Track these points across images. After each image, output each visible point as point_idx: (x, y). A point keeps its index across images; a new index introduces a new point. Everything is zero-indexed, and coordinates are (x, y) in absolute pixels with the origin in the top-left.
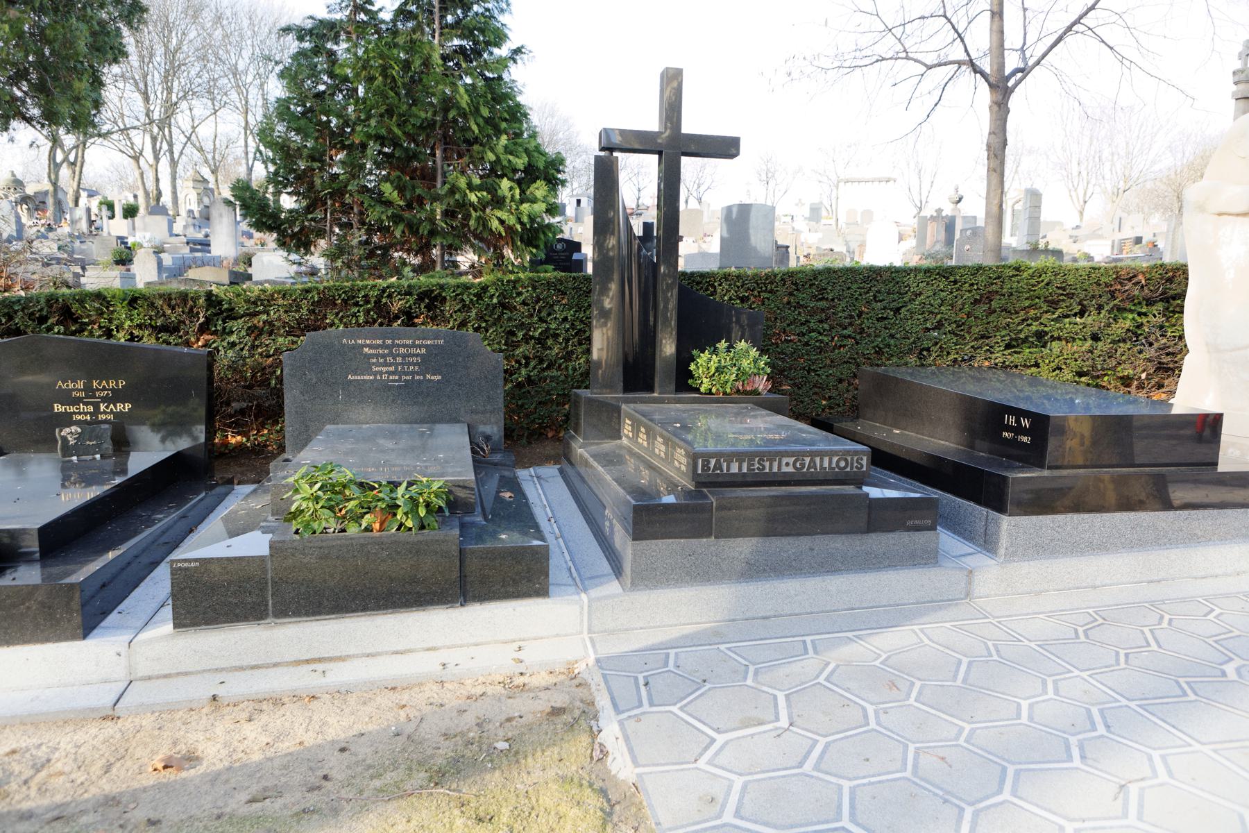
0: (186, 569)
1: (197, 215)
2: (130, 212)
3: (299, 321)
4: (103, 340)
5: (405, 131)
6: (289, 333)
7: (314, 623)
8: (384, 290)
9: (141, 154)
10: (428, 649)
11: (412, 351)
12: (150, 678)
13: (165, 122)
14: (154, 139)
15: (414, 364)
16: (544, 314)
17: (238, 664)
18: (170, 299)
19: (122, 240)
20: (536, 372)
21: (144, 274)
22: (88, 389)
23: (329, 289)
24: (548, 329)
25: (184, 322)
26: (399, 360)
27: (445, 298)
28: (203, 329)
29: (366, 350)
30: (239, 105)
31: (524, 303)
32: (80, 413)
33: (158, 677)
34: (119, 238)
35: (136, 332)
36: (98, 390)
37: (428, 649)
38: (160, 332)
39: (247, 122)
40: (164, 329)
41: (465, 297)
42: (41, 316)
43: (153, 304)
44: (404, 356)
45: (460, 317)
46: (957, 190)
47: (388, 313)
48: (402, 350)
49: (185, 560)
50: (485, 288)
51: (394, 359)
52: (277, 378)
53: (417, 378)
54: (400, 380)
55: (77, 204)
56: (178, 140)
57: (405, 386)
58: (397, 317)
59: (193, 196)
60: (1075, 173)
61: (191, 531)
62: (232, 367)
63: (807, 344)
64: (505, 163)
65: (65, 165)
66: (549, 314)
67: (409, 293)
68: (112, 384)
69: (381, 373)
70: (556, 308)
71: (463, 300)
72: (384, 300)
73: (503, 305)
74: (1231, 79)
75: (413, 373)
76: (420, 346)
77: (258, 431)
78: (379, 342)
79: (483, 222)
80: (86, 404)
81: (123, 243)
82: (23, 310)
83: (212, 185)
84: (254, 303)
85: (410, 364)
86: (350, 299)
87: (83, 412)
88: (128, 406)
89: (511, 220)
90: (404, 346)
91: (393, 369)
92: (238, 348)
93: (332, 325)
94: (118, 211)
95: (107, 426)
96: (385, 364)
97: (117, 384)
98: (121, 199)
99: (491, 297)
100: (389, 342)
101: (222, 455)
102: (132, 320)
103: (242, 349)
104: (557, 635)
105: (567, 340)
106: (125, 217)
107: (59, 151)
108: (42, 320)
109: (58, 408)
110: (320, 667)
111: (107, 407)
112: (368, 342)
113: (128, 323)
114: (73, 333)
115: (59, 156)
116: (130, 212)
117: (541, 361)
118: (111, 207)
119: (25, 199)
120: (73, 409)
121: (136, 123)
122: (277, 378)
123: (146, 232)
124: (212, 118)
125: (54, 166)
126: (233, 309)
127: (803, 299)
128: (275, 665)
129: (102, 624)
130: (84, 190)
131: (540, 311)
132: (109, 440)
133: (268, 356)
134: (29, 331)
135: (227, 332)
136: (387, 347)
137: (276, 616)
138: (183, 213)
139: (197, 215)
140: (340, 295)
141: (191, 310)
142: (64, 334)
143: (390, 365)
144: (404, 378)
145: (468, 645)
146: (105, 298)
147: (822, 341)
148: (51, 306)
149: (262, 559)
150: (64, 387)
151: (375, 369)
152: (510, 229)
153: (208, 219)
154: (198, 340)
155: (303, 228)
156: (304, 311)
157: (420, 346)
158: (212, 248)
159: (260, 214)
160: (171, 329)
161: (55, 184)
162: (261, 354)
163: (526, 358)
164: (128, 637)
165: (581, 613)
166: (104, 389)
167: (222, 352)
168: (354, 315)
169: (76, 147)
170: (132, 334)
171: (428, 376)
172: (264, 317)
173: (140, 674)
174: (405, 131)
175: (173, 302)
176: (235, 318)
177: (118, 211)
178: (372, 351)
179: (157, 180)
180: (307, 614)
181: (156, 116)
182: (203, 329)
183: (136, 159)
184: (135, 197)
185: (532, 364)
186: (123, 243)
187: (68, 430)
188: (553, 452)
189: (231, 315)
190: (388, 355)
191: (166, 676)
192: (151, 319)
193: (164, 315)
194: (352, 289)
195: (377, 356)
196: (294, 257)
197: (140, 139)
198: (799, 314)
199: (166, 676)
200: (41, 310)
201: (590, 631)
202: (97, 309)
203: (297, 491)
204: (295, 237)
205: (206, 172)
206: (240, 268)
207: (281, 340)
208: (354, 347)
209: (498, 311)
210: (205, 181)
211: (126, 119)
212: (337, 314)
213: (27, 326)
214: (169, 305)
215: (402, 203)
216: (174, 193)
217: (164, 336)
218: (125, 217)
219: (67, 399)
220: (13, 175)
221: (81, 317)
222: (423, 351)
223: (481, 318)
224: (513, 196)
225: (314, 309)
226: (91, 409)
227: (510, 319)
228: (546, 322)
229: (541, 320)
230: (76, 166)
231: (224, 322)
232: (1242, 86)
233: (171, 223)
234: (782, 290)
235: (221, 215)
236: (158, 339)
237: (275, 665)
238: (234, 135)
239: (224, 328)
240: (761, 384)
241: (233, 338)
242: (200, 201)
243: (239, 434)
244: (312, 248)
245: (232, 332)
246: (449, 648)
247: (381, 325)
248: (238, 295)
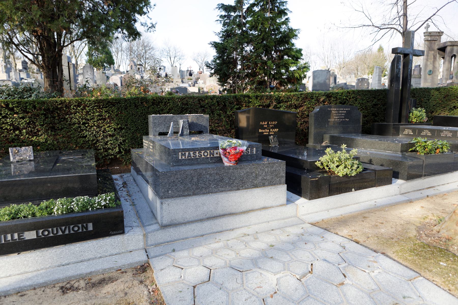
5: (257, 42)
44: (341, 113)
48: (341, 112)
60: (327, 62)
74: (423, 35)
75: (342, 118)
80: (267, 129)
88: (277, 130)
90: (341, 110)
110: (421, 191)
120: (264, 131)
174: (257, 42)
226: (268, 131)
232: (427, 37)
235: (87, 72)
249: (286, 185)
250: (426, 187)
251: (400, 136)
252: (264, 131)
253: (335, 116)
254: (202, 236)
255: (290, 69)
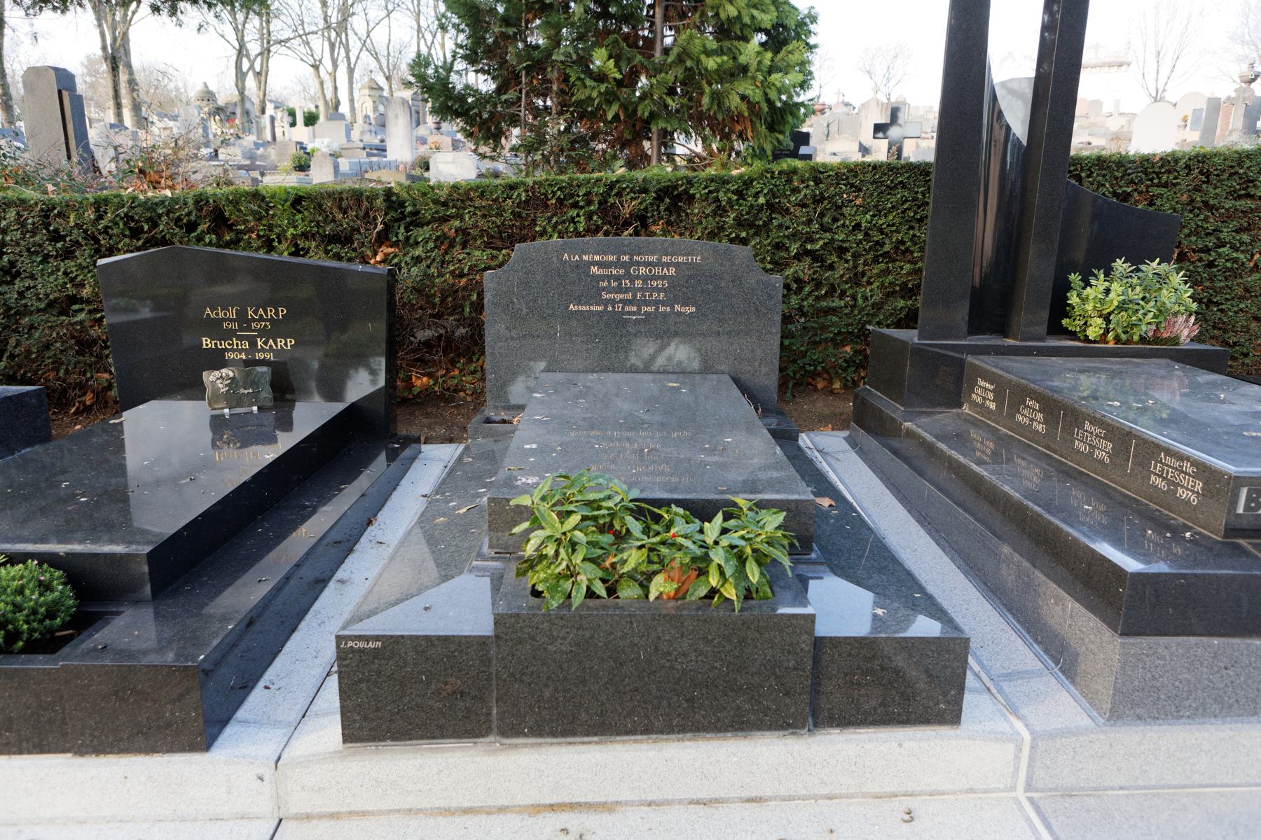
0: (362, 651)
1: (373, 122)
2: (311, 120)
3: (501, 228)
4: (262, 255)
6: (488, 245)
7: (564, 749)
8: (611, 186)
9: (320, 61)
10: (750, 800)
11: (657, 271)
12: (308, 817)
13: (343, 26)
14: (332, 46)
15: (659, 290)
16: (827, 219)
17: (443, 804)
18: (341, 199)
19: (301, 146)
20: (810, 300)
21: (321, 176)
22: (242, 318)
23: (540, 184)
24: (832, 240)
25: (358, 231)
26: (639, 284)
27: (693, 196)
28: (383, 238)
29: (594, 269)
30: (411, 7)
31: (803, 205)
32: (233, 350)
33: (321, 816)
34: (298, 143)
35: (301, 243)
36: (253, 320)
37: (750, 800)
38: (330, 242)
39: (419, 26)
40: (333, 239)
41: (721, 194)
42: (189, 222)
43: (320, 206)
44: (645, 279)
45: (711, 223)
46: (1252, 65)
47: (616, 218)
48: (643, 270)
49: (360, 638)
50: (748, 183)
51: (632, 282)
52: (472, 304)
53: (662, 309)
54: (638, 313)
55: (263, 112)
56: (355, 45)
57: (646, 321)
58: (627, 224)
59: (369, 104)
61: (370, 523)
62: (418, 290)
63: (1211, 265)
64: (747, 20)
65: (251, 73)
66: (835, 220)
67: (645, 190)
68: (271, 312)
69: (613, 302)
70: (846, 211)
71: (717, 200)
72: (611, 200)
73: (770, 206)
75: (657, 303)
76: (668, 265)
77: (448, 371)
78: (611, 258)
79: (717, 98)
80: (241, 338)
81: (302, 148)
82: (167, 215)
83: (386, 93)
84: (445, 204)
85: (653, 289)
86: (567, 198)
87: (236, 350)
88: (291, 342)
89: (755, 94)
90: (647, 264)
91: (629, 296)
92: (424, 264)
93: (543, 233)
94: (300, 119)
95: (265, 369)
96: (619, 290)
97: (277, 313)
98: (302, 106)
99: (756, 195)
100: (626, 258)
101: (405, 401)
102: (295, 227)
103: (429, 267)
104: (971, 791)
105: (856, 256)
106: (307, 124)
107: (245, 61)
108: (191, 227)
109: (207, 343)
111: (266, 343)
112: (597, 258)
113: (291, 230)
114: (227, 245)
115: (246, 65)
116: (311, 120)
117: (818, 285)
118: (292, 114)
119: (219, 110)
120: (224, 345)
121: (315, 29)
122: (472, 304)
123: (322, 140)
124: (386, 21)
125: (240, 76)
126: (418, 213)
127: (1216, 196)
128: (502, 810)
129: (240, 714)
130: (271, 101)
131: (822, 215)
132: (268, 388)
133: (462, 275)
134: (175, 240)
135: (409, 243)
136: (623, 265)
137: (503, 734)
138: (360, 120)
139: (373, 122)
140: (554, 193)
141: (367, 214)
142: (219, 246)
143: (626, 291)
144: (644, 309)
145: (816, 798)
146: (263, 199)
147: (1235, 260)
148: (200, 210)
149: (482, 641)
150: (213, 316)
151: (605, 296)
152: (752, 106)
153: (384, 126)
154: (375, 254)
155: (492, 114)
156: (507, 215)
157: (668, 265)
158: (388, 153)
159: (445, 100)
160: (344, 239)
161: (242, 93)
162: (452, 272)
163: (798, 280)
164: (269, 750)
165: (1017, 758)
166: (261, 319)
167: (404, 270)
168: (572, 220)
169: (261, 54)
170: (296, 245)
171: (677, 308)
172: (457, 223)
173: (293, 811)
175: (344, 203)
176: (421, 225)
177: (300, 119)
178: (601, 272)
179: (336, 88)
180: (554, 735)
181: (334, 20)
182: (383, 238)
183: (316, 67)
184: (317, 107)
185: (807, 289)
186: (302, 148)
187: (217, 373)
188: (826, 411)
189: (416, 221)
190: (624, 277)
191: (333, 816)
192: (318, 226)
193: (334, 221)
194: (570, 185)
195: (609, 278)
196: (484, 149)
197: (319, 45)
198: (1206, 220)
199: (333, 816)
200: (189, 214)
201: (1029, 787)
202: (253, 213)
203: (537, 525)
204: (482, 122)
205: (382, 81)
206: (418, 172)
207: (477, 253)
208: (577, 266)
209: (764, 216)
210: (381, 89)
211: (306, 26)
212: (550, 219)
213: (174, 235)
214: (340, 208)
215: (618, 76)
216: (352, 100)
217: (336, 248)
218: (307, 124)
219: (215, 329)
220: (206, 86)
221: (237, 223)
222: (672, 271)
223: (739, 223)
224: (760, 63)
225: (502, 219)
227: (780, 226)
228: (830, 230)
229: (824, 228)
230: (261, 76)
231: (407, 230)
233: (349, 129)
234: (1184, 183)
235: (396, 116)
236: (327, 252)
237: (502, 810)
238: (407, 39)
239: (408, 238)
240: (1185, 330)
241: (419, 252)
242: (375, 109)
243: (424, 375)
244: (503, 141)
245: (417, 243)
246: (783, 799)
247: (606, 234)
248: (424, 194)
249: (484, 626)
250: (521, 799)
251: (966, 408)
252: (224, 345)
253: (610, 290)
254: (830, 798)
255: (494, 86)
